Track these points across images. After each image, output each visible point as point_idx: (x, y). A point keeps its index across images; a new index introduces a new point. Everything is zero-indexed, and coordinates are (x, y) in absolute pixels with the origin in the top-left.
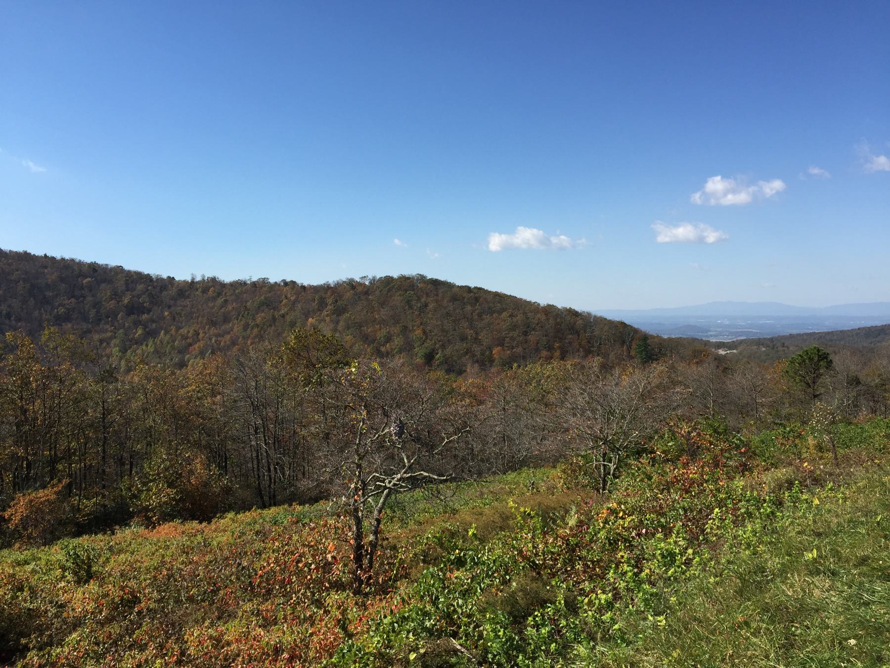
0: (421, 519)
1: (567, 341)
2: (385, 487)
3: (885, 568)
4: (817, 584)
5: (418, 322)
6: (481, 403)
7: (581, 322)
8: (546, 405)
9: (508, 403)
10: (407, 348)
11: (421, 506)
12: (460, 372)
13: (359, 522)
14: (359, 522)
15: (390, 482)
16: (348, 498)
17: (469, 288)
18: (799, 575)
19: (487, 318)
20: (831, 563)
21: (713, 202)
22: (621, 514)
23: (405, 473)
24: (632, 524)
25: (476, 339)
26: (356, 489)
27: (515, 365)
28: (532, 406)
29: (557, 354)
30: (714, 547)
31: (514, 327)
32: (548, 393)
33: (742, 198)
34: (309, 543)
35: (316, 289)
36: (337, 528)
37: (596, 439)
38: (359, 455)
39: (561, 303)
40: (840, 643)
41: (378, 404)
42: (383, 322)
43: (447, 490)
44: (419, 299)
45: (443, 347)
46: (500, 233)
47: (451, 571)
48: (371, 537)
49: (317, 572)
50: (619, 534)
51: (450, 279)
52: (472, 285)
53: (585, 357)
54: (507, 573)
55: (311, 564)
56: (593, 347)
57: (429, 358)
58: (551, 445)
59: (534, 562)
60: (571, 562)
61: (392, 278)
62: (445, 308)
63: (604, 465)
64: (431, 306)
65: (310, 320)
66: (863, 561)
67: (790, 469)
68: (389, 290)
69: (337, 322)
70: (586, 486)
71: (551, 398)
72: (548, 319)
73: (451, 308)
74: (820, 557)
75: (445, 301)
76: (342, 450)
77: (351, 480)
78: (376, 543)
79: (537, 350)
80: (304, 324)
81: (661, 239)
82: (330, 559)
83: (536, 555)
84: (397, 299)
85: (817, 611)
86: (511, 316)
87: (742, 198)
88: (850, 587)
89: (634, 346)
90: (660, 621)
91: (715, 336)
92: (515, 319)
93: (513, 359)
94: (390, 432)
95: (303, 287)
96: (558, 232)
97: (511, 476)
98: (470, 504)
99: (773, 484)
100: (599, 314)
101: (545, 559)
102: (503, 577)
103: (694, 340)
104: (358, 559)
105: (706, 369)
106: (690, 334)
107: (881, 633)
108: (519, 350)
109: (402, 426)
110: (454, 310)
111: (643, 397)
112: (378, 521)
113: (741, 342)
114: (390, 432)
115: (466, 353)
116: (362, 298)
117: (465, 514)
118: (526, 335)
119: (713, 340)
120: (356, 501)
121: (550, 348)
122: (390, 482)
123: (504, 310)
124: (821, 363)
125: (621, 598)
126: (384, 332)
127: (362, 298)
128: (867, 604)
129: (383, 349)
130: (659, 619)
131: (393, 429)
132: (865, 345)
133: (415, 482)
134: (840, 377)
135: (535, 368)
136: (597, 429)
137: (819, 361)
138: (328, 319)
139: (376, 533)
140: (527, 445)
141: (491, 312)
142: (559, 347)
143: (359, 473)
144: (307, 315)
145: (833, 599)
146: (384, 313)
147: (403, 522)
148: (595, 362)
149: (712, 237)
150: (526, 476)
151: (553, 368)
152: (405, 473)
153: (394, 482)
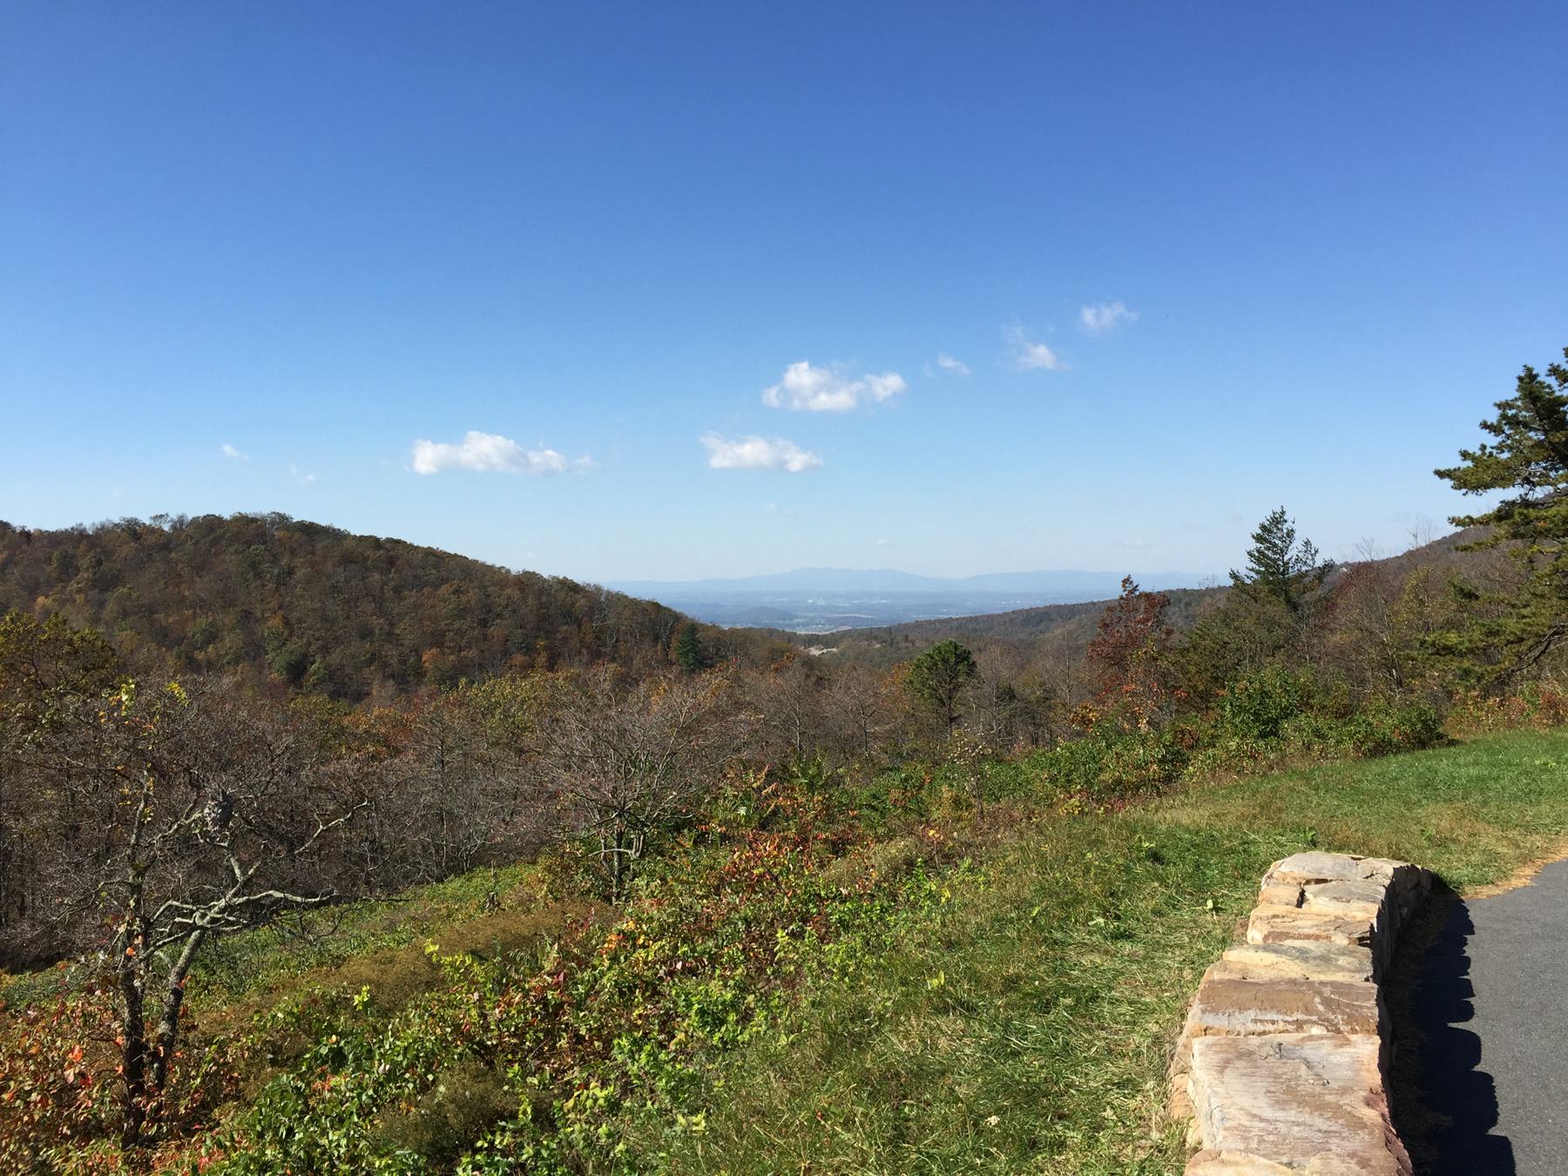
0: (271, 982)
1: (559, 636)
2: (194, 927)
3: (1043, 993)
4: (944, 1028)
5: (274, 604)
6: (397, 752)
7: (583, 601)
8: (520, 751)
9: (450, 750)
10: (253, 652)
11: (270, 957)
12: (360, 696)
13: (135, 1000)
14: (135, 1000)
15: (203, 916)
16: (113, 953)
17: (376, 540)
18: (918, 1016)
19: (411, 597)
20: (964, 990)
21: (797, 404)
22: (641, 941)
23: (235, 895)
24: (661, 955)
25: (390, 634)
26: (130, 935)
27: (463, 680)
28: (495, 753)
29: (542, 659)
30: (790, 982)
31: (462, 612)
32: (525, 729)
33: (841, 400)
34: (25, 1050)
35: (54, 540)
36: (86, 1016)
37: (606, 808)
38: (135, 867)
39: (548, 568)
40: (976, 1125)
41: (175, 766)
42: (200, 605)
43: (322, 923)
44: (275, 560)
45: (325, 650)
46: (435, 442)
47: (323, 1076)
48: (163, 1027)
49: (44, 1107)
50: (636, 976)
51: (339, 525)
52: (382, 535)
53: (591, 663)
54: (428, 1071)
55: (29, 1093)
56: (605, 645)
57: (297, 671)
58: (525, 824)
59: (481, 1044)
60: (552, 1035)
61: (219, 519)
62: (329, 577)
63: (619, 854)
64: (300, 573)
65: (41, 600)
66: (1011, 984)
67: (910, 840)
68: (214, 543)
69: (102, 605)
70: (589, 891)
71: (528, 740)
72: (525, 598)
73: (342, 577)
74: (949, 981)
75: (330, 564)
76: (98, 859)
77: (118, 918)
78: (172, 1039)
79: (506, 653)
80: (28, 608)
81: (717, 462)
82: (71, 1079)
83: (486, 1029)
84: (230, 560)
85: (943, 1073)
86: (457, 592)
87: (841, 400)
88: (992, 1029)
89: (674, 644)
90: (697, 1124)
91: (805, 625)
92: (464, 598)
93: (462, 669)
94: (202, 820)
95: (26, 535)
96: (541, 444)
97: (454, 885)
98: (368, 942)
99: (884, 868)
100: (615, 589)
101: (500, 1037)
102: (423, 1078)
103: (771, 632)
104: (134, 1072)
105: (791, 681)
106: (766, 622)
107: (1035, 1102)
108: (472, 653)
109: (228, 806)
110: (347, 581)
111: (686, 731)
112: (178, 994)
113: (845, 634)
114: (202, 820)
115: (371, 661)
116: (156, 556)
117: (360, 964)
118: (485, 626)
119: (802, 632)
120: (128, 958)
121: (529, 649)
122: (203, 916)
123: (444, 581)
124: (960, 667)
125: (632, 1091)
126: (203, 622)
127: (156, 556)
128: (1015, 1054)
129: (200, 656)
130: (695, 1119)
131: (209, 811)
132: (1022, 636)
133: (258, 913)
134: (987, 688)
135: (503, 688)
136: (607, 789)
137: (957, 663)
138: (80, 598)
139: (172, 1018)
140: (485, 826)
141: (419, 584)
142: (546, 648)
143: (137, 902)
144: (34, 589)
145: (967, 1051)
146: (202, 586)
147: (235, 990)
148: (605, 674)
149: (797, 461)
150: (483, 879)
151: (532, 685)
152: (235, 895)
153: (212, 914)
